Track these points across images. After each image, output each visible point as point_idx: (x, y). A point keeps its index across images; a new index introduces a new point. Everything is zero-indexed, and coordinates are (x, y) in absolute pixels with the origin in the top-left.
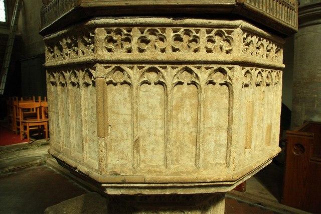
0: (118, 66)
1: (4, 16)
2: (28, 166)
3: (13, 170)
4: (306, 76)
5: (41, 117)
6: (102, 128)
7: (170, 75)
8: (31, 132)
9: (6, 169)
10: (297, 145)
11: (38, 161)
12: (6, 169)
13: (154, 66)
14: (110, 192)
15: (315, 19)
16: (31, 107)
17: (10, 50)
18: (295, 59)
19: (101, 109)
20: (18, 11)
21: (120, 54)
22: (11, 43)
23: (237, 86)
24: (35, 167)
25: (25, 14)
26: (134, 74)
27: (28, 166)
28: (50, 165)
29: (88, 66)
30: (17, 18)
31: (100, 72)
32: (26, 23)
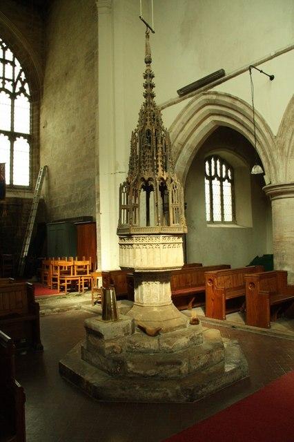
0: (138, 244)
1: (28, 181)
2: (69, 309)
3: (59, 311)
4: (278, 237)
5: (74, 274)
6: (134, 257)
7: (147, 246)
8: (68, 286)
9: (54, 310)
10: (251, 283)
11: (76, 306)
12: (54, 310)
13: (145, 245)
14: (136, 271)
15: (277, 195)
16: (64, 266)
17: (34, 213)
18: (98, 251)
19: (134, 254)
20: (43, 176)
21: (138, 242)
22: (35, 206)
23: (161, 248)
24: (73, 310)
25: (48, 179)
26: (141, 246)
27: (69, 309)
28: (85, 309)
29: (132, 245)
30: (41, 183)
31: (134, 246)
32: (49, 187)
